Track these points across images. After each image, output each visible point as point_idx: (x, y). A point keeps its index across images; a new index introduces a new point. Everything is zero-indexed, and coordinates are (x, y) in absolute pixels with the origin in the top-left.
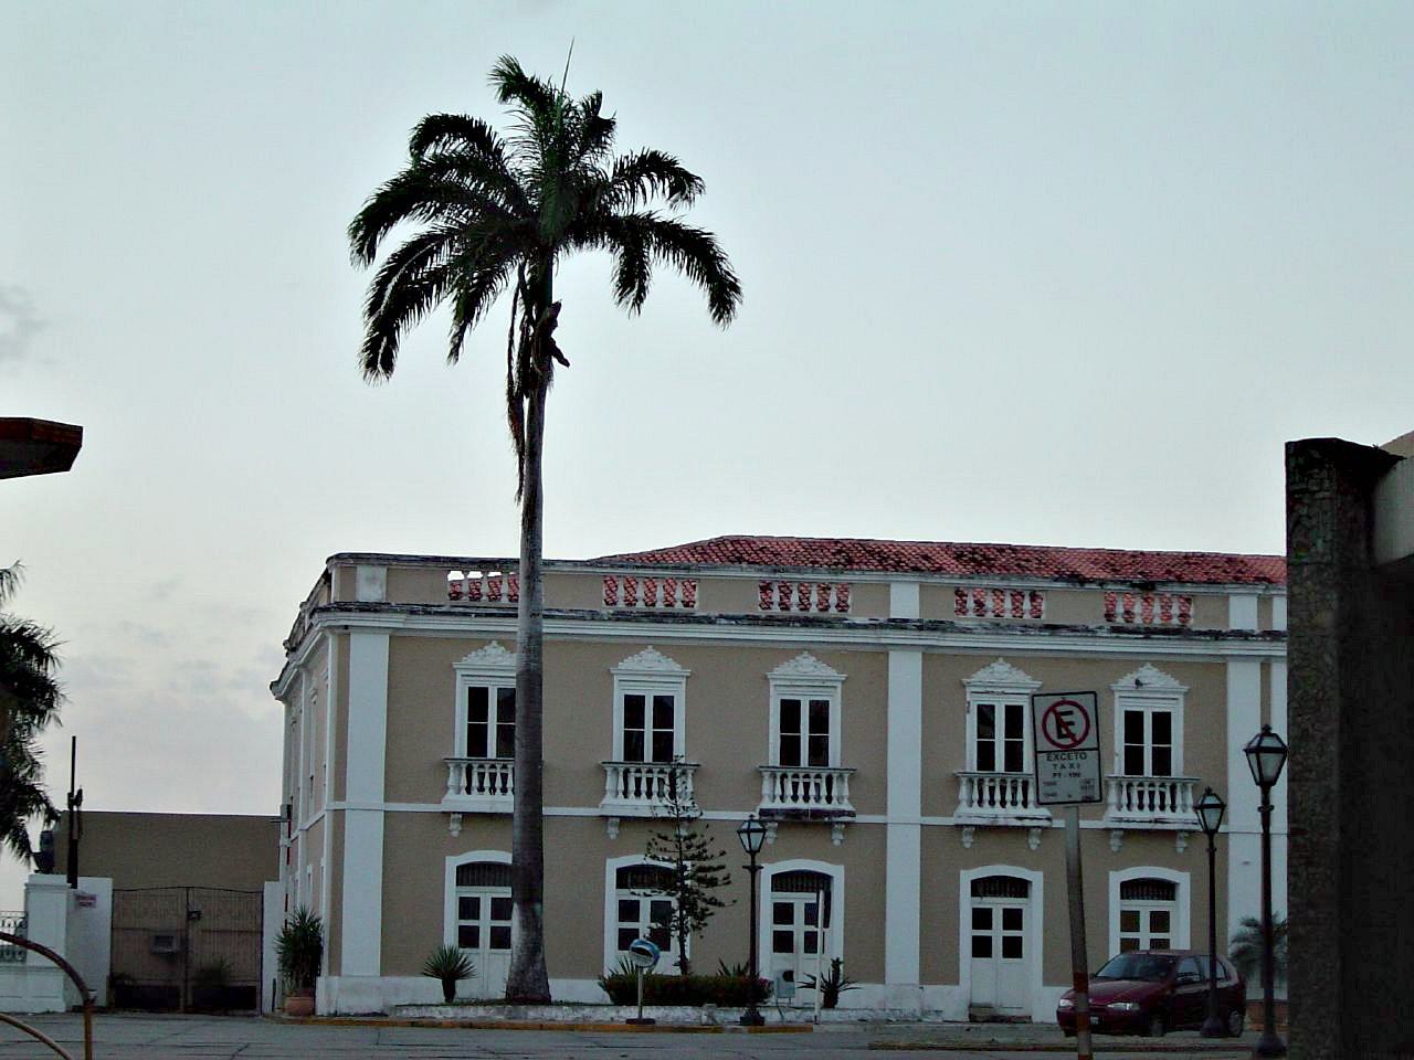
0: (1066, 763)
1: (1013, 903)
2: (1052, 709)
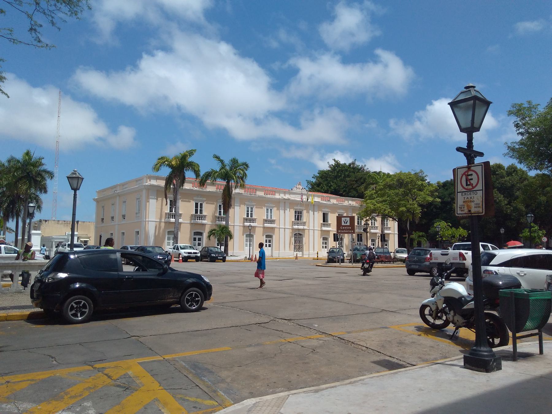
0: (469, 196)
1: (200, 237)
2: (464, 174)
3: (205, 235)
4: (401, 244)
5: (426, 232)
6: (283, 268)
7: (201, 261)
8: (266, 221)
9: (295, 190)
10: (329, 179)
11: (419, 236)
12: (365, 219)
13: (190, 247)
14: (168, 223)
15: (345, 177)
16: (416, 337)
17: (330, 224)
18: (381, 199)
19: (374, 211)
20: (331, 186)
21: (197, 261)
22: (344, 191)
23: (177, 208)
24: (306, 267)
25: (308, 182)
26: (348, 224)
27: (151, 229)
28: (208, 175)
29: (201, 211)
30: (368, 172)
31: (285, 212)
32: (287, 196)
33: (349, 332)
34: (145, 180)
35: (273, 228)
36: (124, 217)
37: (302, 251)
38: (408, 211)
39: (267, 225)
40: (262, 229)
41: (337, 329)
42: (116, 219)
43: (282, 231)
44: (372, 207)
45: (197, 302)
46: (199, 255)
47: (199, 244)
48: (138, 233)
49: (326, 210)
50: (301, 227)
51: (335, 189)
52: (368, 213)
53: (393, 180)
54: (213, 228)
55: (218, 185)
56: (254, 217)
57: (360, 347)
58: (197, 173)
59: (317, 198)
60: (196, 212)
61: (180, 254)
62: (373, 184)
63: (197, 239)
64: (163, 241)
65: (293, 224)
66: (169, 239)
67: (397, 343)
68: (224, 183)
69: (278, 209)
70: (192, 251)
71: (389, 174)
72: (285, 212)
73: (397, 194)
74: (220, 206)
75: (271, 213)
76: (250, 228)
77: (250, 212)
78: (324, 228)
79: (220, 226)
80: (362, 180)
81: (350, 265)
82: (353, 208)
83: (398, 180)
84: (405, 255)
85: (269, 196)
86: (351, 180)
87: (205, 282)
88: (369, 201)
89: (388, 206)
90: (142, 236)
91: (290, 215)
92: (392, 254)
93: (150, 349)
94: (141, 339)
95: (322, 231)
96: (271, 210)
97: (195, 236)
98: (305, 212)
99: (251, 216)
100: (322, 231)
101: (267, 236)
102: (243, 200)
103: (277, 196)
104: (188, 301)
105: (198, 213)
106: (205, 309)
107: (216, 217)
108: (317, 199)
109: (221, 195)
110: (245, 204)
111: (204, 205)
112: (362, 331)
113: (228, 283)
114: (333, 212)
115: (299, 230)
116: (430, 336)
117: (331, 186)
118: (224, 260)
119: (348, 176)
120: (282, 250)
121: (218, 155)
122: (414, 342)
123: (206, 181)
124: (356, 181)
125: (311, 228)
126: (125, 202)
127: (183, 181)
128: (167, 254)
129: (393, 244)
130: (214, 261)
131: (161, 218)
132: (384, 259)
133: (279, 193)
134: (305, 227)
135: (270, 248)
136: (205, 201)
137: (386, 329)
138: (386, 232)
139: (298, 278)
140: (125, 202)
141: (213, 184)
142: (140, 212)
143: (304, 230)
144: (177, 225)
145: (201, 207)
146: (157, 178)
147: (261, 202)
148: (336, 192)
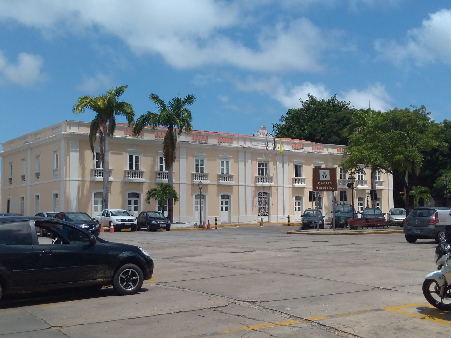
1: (135, 199)
4: (398, 202)
5: (431, 187)
7: (139, 230)
8: (221, 177)
10: (302, 121)
11: (421, 193)
15: (322, 118)
16: (418, 321)
17: (304, 179)
18: (370, 145)
20: (305, 129)
22: (322, 136)
23: (106, 164)
26: (328, 178)
27: (73, 191)
28: (145, 120)
29: (137, 166)
30: (353, 111)
31: (245, 165)
32: (248, 144)
33: (331, 317)
34: (63, 126)
35: (230, 186)
36: (38, 175)
38: (406, 159)
41: (315, 312)
42: (28, 178)
44: (359, 155)
45: (135, 282)
46: (135, 222)
47: (135, 209)
48: (56, 195)
50: (267, 184)
51: (310, 134)
52: (352, 164)
56: (205, 172)
57: (346, 334)
59: (286, 146)
60: (131, 167)
61: (111, 222)
62: (359, 126)
63: (133, 203)
65: (257, 179)
67: (395, 329)
68: (166, 129)
69: (237, 161)
70: (127, 218)
72: (245, 165)
73: (391, 138)
74: (161, 159)
75: (227, 166)
77: (200, 166)
78: (297, 185)
79: (161, 185)
80: (345, 121)
81: (332, 231)
82: (334, 158)
83: (393, 120)
84: (403, 218)
85: (224, 144)
86: (330, 122)
87: (144, 256)
89: (380, 154)
91: (250, 169)
92: (386, 216)
94: (64, 330)
95: (294, 188)
96: (227, 162)
97: (130, 199)
98: (271, 165)
99: (202, 171)
100: (294, 188)
101: (223, 197)
104: (123, 281)
106: (145, 290)
107: (156, 173)
108: (287, 147)
110: (193, 156)
112: (349, 314)
114: (308, 164)
115: (264, 187)
116: (437, 320)
117: (305, 129)
118: (168, 228)
119: (327, 116)
120: (242, 215)
121: (156, 94)
122: (416, 328)
124: (338, 122)
125: (280, 184)
126: (38, 156)
128: (94, 222)
129: (387, 203)
130: (156, 230)
131: (83, 175)
134: (272, 184)
136: (142, 152)
138: (378, 187)
139: (264, 249)
140: (38, 156)
142: (58, 169)
143: (270, 187)
144: (107, 185)
145: (137, 161)
146: (79, 124)
148: (311, 138)
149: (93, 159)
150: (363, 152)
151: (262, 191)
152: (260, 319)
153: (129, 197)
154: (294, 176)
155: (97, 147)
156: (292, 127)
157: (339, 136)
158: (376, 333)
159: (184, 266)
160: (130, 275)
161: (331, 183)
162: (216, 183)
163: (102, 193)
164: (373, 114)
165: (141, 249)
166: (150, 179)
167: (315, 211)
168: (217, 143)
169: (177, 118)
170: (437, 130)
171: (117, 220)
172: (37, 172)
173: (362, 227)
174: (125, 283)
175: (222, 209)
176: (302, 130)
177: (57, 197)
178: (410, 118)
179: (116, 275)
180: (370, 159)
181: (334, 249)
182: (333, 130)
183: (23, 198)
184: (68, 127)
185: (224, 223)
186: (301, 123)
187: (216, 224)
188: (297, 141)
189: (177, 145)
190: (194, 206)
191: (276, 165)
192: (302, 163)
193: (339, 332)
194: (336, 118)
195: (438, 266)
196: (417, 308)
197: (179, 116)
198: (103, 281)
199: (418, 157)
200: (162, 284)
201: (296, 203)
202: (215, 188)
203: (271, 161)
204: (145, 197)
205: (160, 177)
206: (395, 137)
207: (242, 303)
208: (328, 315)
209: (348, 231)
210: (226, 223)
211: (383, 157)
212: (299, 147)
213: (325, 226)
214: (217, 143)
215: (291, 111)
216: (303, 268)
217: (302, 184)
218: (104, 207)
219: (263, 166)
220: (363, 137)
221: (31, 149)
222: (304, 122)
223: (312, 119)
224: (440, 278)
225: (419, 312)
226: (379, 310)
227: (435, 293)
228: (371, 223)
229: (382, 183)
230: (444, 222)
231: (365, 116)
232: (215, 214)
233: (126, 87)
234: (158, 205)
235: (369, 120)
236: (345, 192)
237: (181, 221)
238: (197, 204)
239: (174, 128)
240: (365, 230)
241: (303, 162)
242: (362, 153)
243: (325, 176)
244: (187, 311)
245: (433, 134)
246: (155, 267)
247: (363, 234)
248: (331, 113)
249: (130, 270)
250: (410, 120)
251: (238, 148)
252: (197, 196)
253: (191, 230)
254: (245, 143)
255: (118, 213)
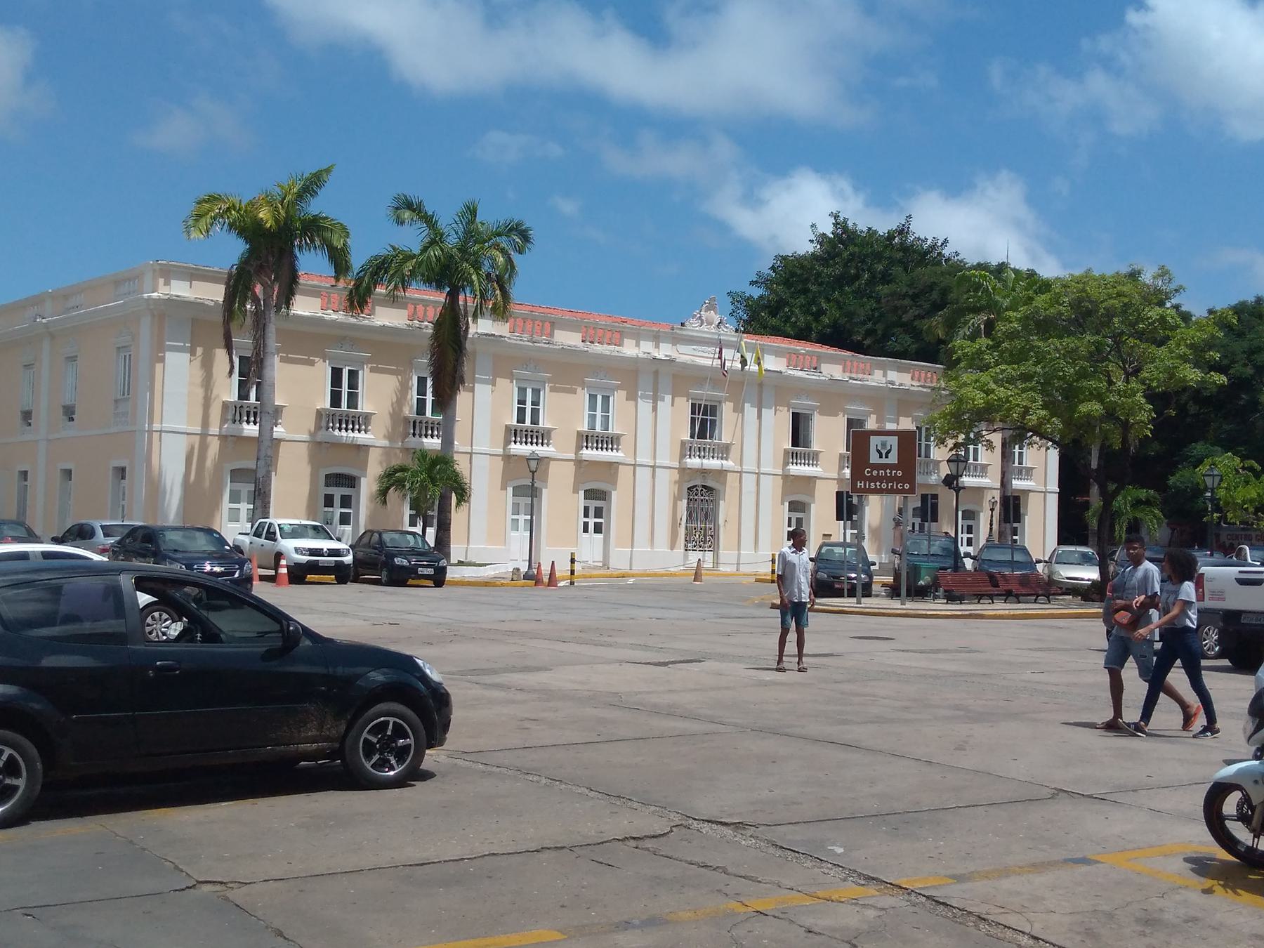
1: (346, 491)
3: (368, 486)
4: (1071, 528)
5: (1161, 487)
6: (660, 613)
7: (356, 580)
8: (586, 439)
9: (693, 324)
10: (814, 288)
11: (1137, 503)
12: (950, 442)
13: (315, 528)
14: (231, 441)
15: (872, 281)
16: (1196, 897)
17: (816, 454)
18: (1010, 370)
19: (985, 414)
20: (821, 312)
21: (342, 580)
22: (869, 333)
23: (266, 387)
24: (737, 612)
25: (735, 298)
26: (893, 458)
27: (171, 462)
28: (380, 268)
29: (353, 399)
30: (956, 267)
31: (655, 409)
32: (664, 351)
33: (960, 878)
34: (148, 279)
35: (612, 467)
36: (69, 413)
37: (715, 549)
38: (1110, 414)
39: (589, 454)
40: (571, 468)
41: (914, 861)
42: (42, 416)
43: (643, 475)
44: (979, 399)
45: (401, 754)
46: (348, 559)
47: (345, 520)
48: (121, 472)
49: (802, 404)
50: (713, 463)
51: (835, 325)
52: (964, 421)
53: (1056, 300)
54: (396, 462)
55: (416, 302)
56: (544, 423)
57: (1009, 933)
58: (339, 260)
59: (775, 358)
60: (336, 401)
61: (279, 556)
62: (976, 310)
63: (337, 501)
64: (216, 504)
65: (686, 450)
66: (235, 498)
67: (1138, 921)
68: (440, 297)
69: (632, 397)
70: (326, 545)
71: (1032, 274)
72: (655, 409)
73: (1071, 354)
74: (422, 381)
75: (606, 408)
76: (533, 464)
77: (529, 407)
78: (795, 469)
79: (423, 454)
80: (935, 295)
81: (895, 604)
82: (903, 401)
83: (1076, 305)
84: (1090, 574)
85: (599, 348)
86: (893, 294)
87: (424, 678)
88: (965, 377)
89: (1038, 397)
90: (137, 486)
91: (673, 418)
92: (1040, 567)
93: (280, 934)
94: (237, 895)
95: (786, 477)
96: (606, 399)
97: (330, 490)
98: (727, 410)
99: (535, 420)
100: (786, 477)
101: (590, 494)
102: (507, 362)
103: (630, 349)
104: (369, 749)
105: (342, 408)
106: (427, 776)
107: (406, 420)
108: (772, 363)
109: (426, 343)
110: (511, 377)
111: (365, 376)
112: (1005, 872)
113: (474, 672)
114: (829, 411)
115: (704, 472)
116: (1246, 896)
117: (821, 312)
118: (439, 579)
119: (886, 278)
120: (642, 547)
121: (414, 194)
122: (1194, 920)
123: (369, 291)
124: (914, 297)
125: (750, 465)
126: (73, 359)
127: (289, 289)
128: (233, 556)
129: (1040, 531)
130: (401, 583)
131: (205, 423)
132: (1015, 588)
133: (637, 337)
134: (728, 464)
135: (600, 536)
136: (369, 361)
137: (1085, 869)
138: (1017, 484)
139: (722, 657)
140: (73, 359)
141: (393, 301)
142: (130, 396)
143: (722, 473)
144: (267, 448)
145: (353, 385)
146: (194, 275)
147: (571, 371)
148: (838, 338)
149: (231, 372)
150: (993, 391)
151: (699, 482)
152: (768, 879)
153: (327, 485)
154: (788, 445)
155: (243, 342)
156: (787, 304)
157: (916, 334)
158: (1090, 933)
159: (513, 702)
160: (389, 733)
161: (900, 474)
162: (572, 456)
163: (255, 471)
164: (1016, 280)
165: (420, 662)
166: (390, 437)
167: (850, 546)
168: (581, 345)
169: (472, 271)
170: (1199, 336)
171: (297, 550)
172: (68, 403)
173: (979, 597)
174: (377, 757)
175: (586, 530)
176: (812, 314)
177: (123, 478)
178: (1127, 300)
179: (353, 733)
180: (1009, 410)
181: (914, 664)
182: (900, 317)
183: (24, 474)
184: (161, 281)
185: (589, 568)
186: (810, 295)
187: (572, 572)
188: (802, 347)
189: (468, 346)
190: (510, 517)
191: (742, 411)
192: (813, 408)
193: (990, 925)
194: (910, 285)
195: (1254, 748)
196: (1187, 860)
197: (477, 266)
198: (317, 749)
199: (1141, 408)
200: (465, 756)
201: (790, 519)
202: (571, 468)
203: (727, 399)
204: (375, 487)
205: (417, 432)
206: (1083, 351)
207: (706, 828)
208: (950, 872)
209: (938, 606)
210: (595, 568)
211: (1044, 407)
212: (807, 364)
213: (876, 588)
214: (581, 345)
215: (784, 258)
216: (845, 722)
217: (811, 468)
218: (259, 511)
219: (705, 413)
220: (992, 347)
221: (52, 336)
222: (820, 292)
223: (841, 287)
224: (1256, 782)
225: (1192, 870)
226: (1084, 861)
227: (1238, 820)
228: (1003, 587)
229: (1029, 471)
230: (1219, 599)
231: (991, 283)
232: (566, 543)
233: (328, 171)
234: (407, 512)
235: (1004, 297)
236: (935, 496)
237: (471, 558)
238: (516, 511)
239: (461, 297)
240: (985, 607)
241: (818, 407)
242: (988, 392)
243: (884, 452)
244: (562, 848)
245: (1187, 346)
246: (457, 715)
247: (982, 617)
248: (897, 270)
249: (392, 720)
250: (1125, 304)
251: (636, 360)
252: (518, 492)
253: (502, 585)
254: (657, 347)
255: (297, 532)
